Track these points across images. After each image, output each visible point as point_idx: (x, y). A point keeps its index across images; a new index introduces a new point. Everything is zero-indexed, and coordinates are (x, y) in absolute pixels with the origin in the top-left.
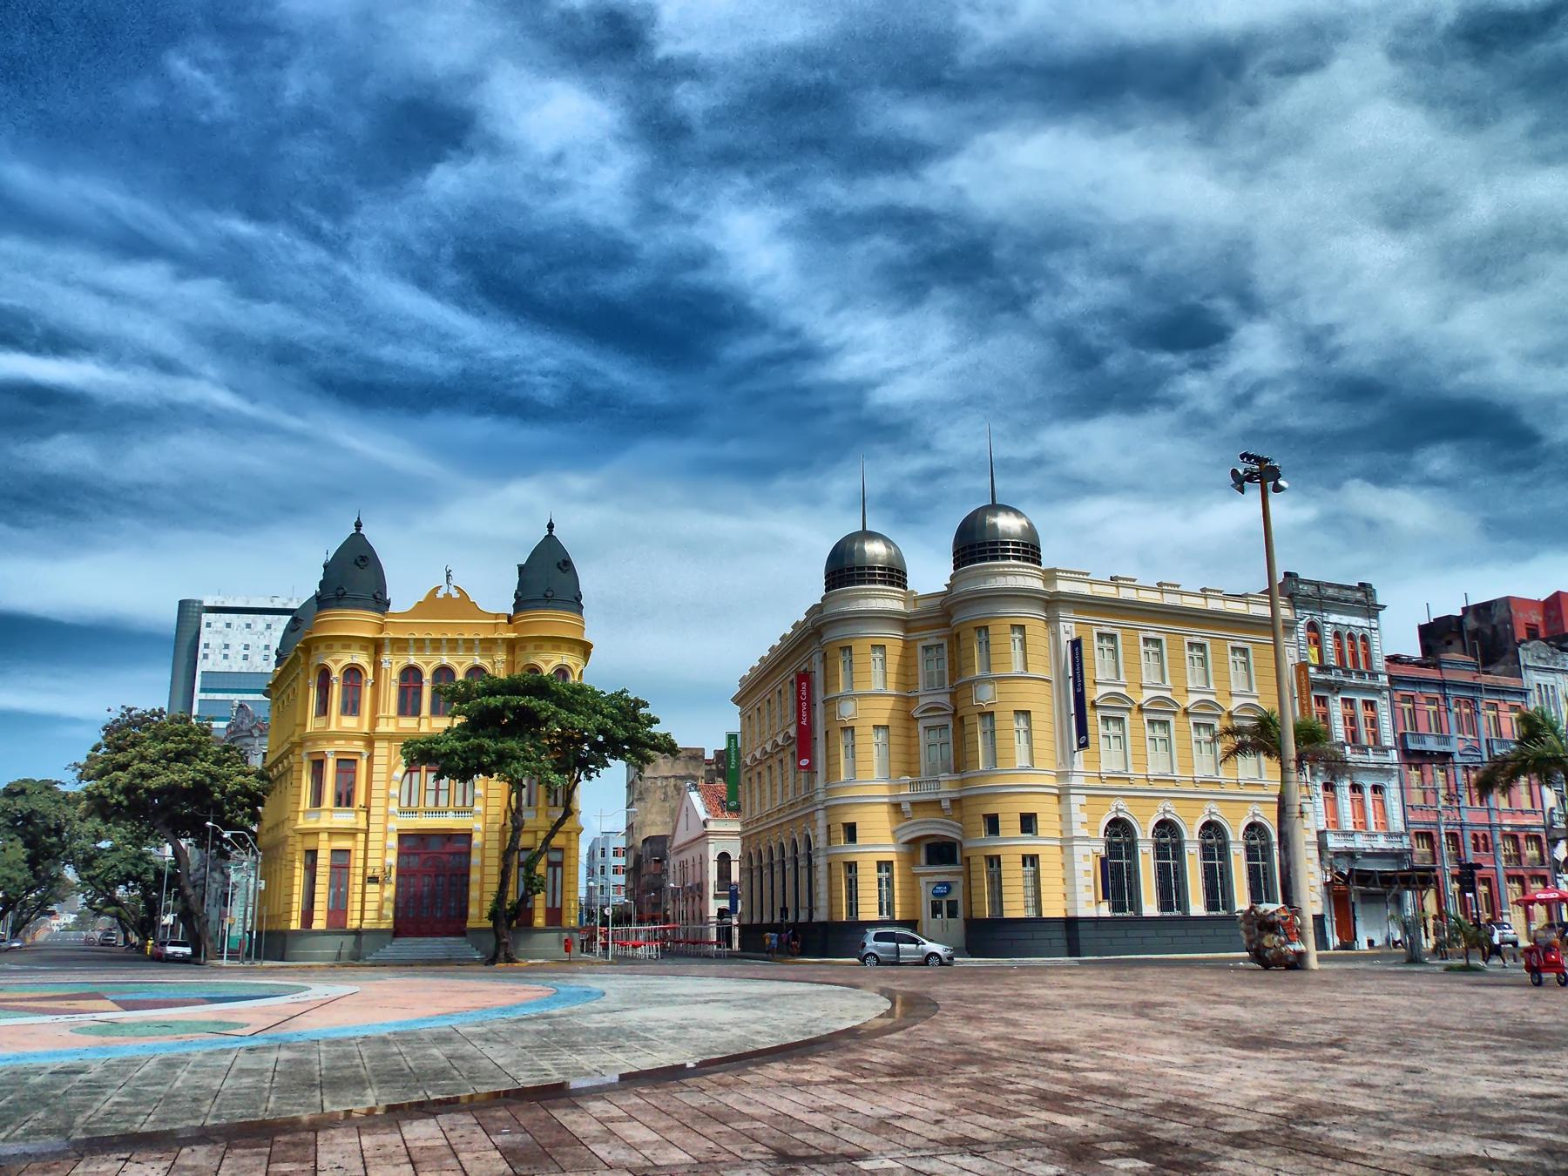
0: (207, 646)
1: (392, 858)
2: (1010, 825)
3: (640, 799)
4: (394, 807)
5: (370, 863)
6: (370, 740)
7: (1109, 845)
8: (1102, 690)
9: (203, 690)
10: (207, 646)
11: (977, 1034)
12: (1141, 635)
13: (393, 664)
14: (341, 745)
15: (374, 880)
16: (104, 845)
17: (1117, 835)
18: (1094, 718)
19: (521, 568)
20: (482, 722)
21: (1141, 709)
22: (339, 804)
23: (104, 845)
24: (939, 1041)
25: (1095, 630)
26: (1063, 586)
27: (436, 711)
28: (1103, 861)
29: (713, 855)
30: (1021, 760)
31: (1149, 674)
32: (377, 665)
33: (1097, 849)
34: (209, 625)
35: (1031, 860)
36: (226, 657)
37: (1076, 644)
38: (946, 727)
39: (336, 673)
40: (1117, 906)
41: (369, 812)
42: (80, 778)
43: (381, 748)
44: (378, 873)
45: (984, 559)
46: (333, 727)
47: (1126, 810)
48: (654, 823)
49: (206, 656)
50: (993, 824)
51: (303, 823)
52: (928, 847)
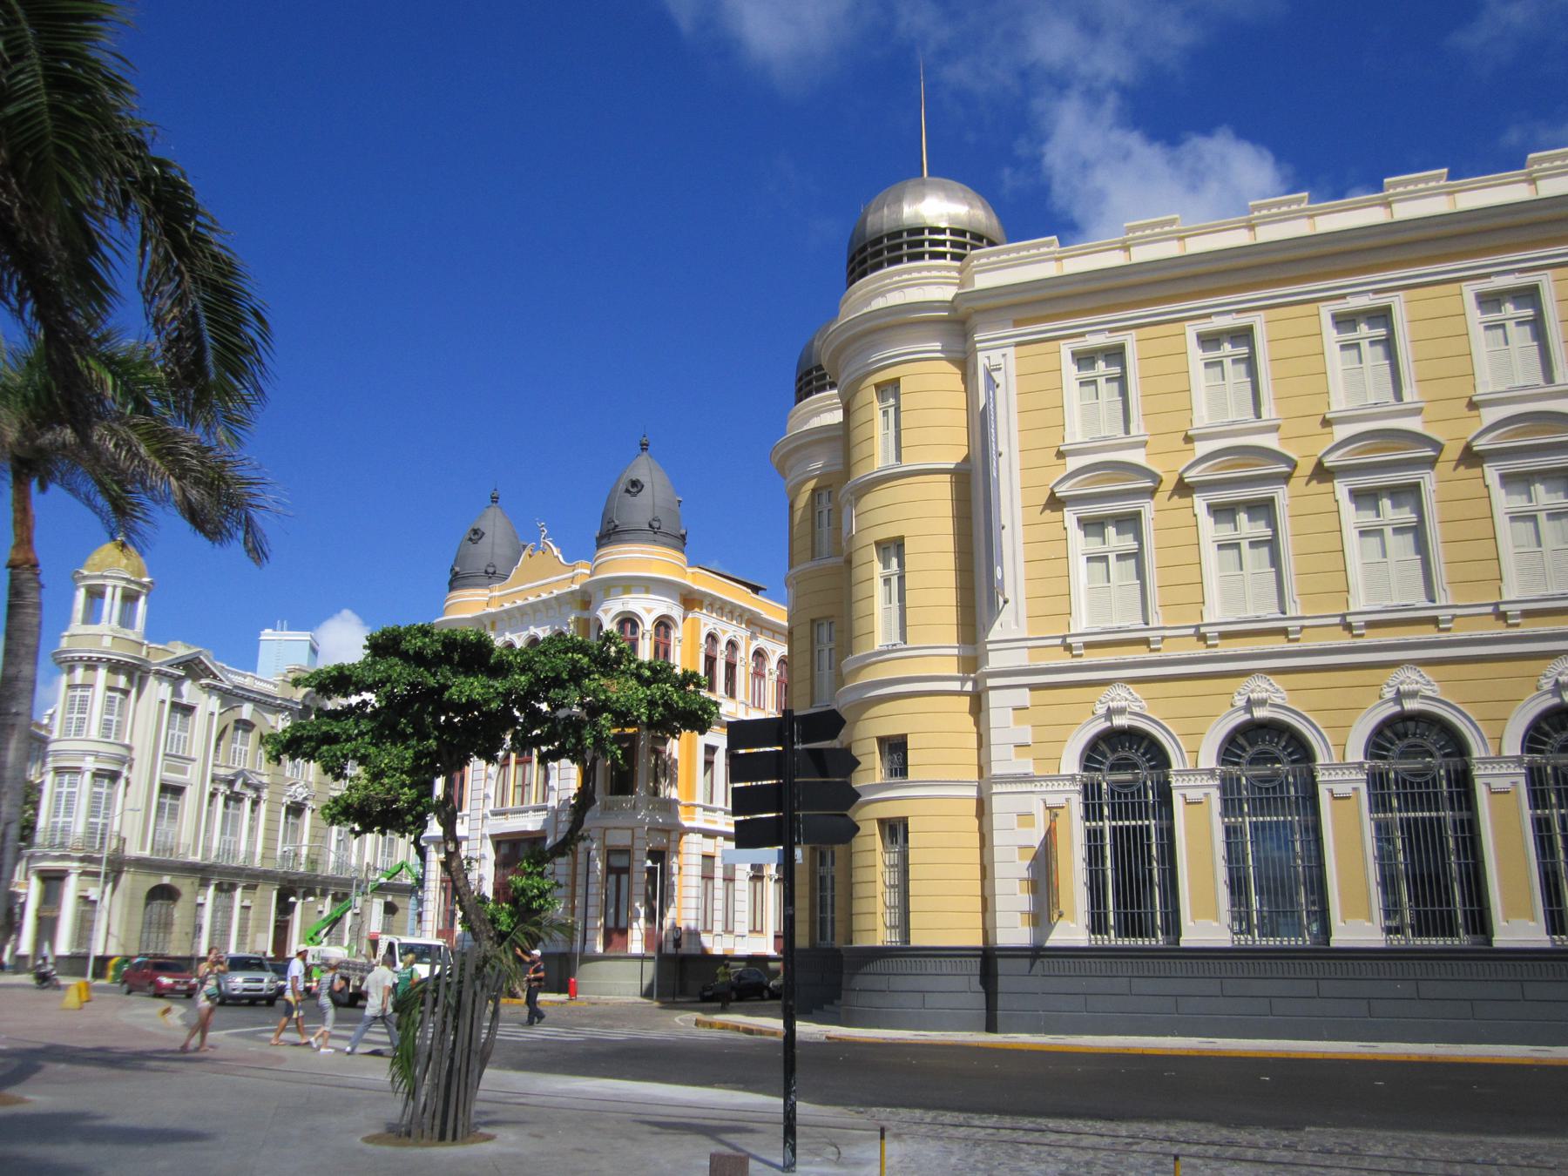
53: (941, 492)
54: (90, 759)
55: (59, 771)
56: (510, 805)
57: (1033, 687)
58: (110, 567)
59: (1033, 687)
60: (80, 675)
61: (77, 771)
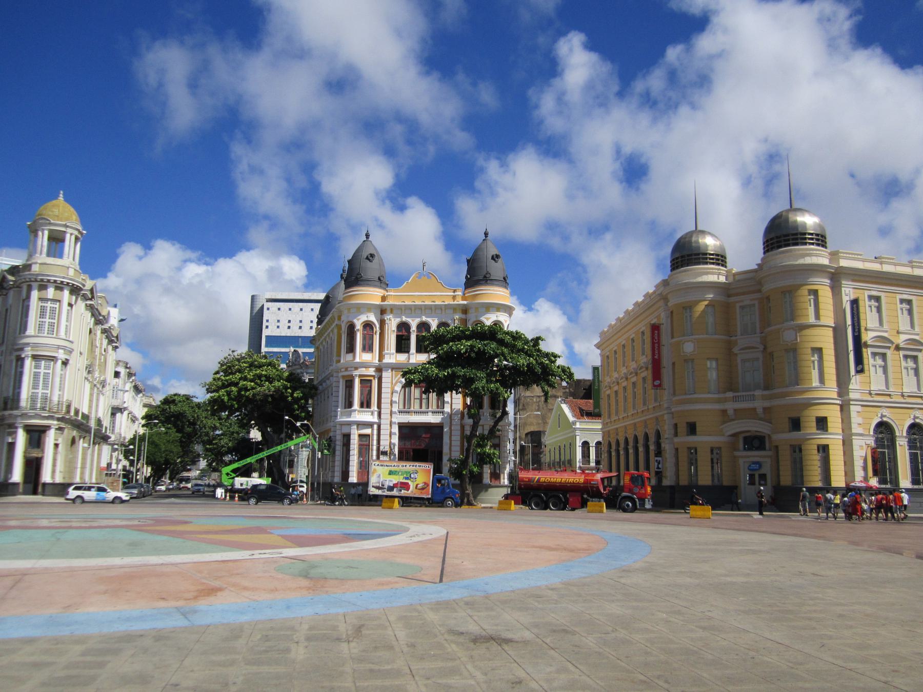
0: (267, 321)
1: (395, 440)
2: (810, 427)
3: (524, 409)
5: (382, 443)
6: (379, 370)
7: (877, 441)
8: (871, 334)
9: (267, 346)
10: (267, 321)
12: (899, 297)
13: (392, 323)
14: (363, 371)
15: (385, 453)
16: (218, 432)
17: (881, 433)
18: (867, 353)
19: (468, 261)
20: (443, 361)
21: (898, 348)
22: (362, 406)
23: (218, 432)
25: (867, 293)
26: (844, 263)
27: (419, 350)
28: (874, 452)
29: (579, 443)
30: (815, 383)
31: (903, 322)
32: (382, 323)
33: (868, 442)
34: (268, 309)
36: (278, 327)
37: (855, 303)
38: (757, 359)
39: (359, 326)
40: (882, 481)
41: (382, 410)
42: (208, 391)
43: (387, 375)
45: (788, 245)
46: (357, 360)
47: (889, 416)
48: (532, 424)
49: (267, 327)
50: (796, 424)
51: (341, 419)
52: (745, 439)
53: (830, 333)
54: (61, 351)
55: (35, 357)
56: (412, 409)
57: (862, 406)
58: (67, 219)
59: (862, 406)
60: (51, 292)
61: (53, 359)
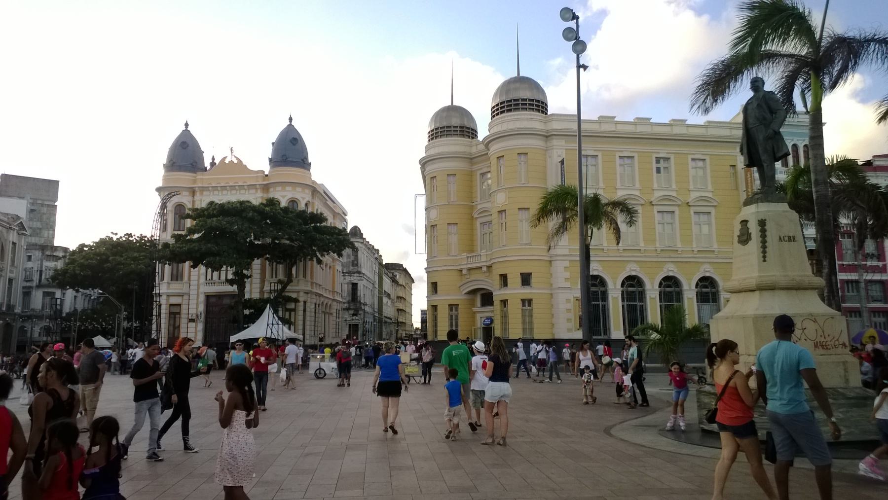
1: (202, 308)
4: (202, 280)
11: (471, 404)
12: (690, 157)
15: (192, 320)
24: (806, 385)
35: (527, 302)
44: (194, 317)
